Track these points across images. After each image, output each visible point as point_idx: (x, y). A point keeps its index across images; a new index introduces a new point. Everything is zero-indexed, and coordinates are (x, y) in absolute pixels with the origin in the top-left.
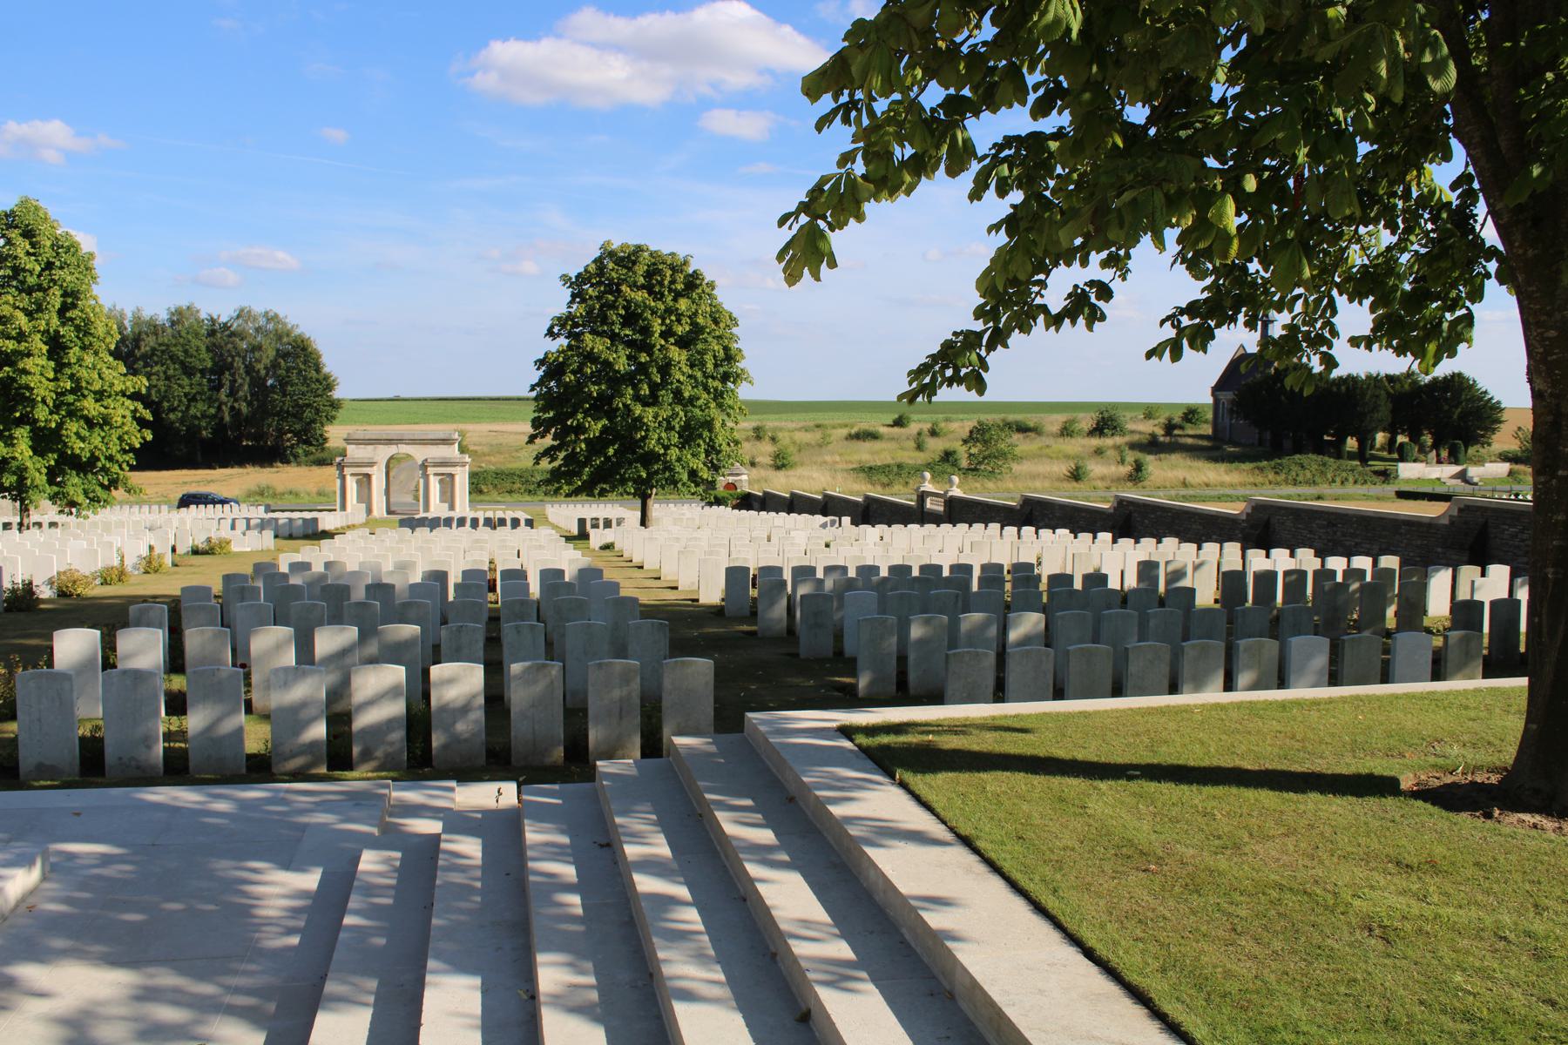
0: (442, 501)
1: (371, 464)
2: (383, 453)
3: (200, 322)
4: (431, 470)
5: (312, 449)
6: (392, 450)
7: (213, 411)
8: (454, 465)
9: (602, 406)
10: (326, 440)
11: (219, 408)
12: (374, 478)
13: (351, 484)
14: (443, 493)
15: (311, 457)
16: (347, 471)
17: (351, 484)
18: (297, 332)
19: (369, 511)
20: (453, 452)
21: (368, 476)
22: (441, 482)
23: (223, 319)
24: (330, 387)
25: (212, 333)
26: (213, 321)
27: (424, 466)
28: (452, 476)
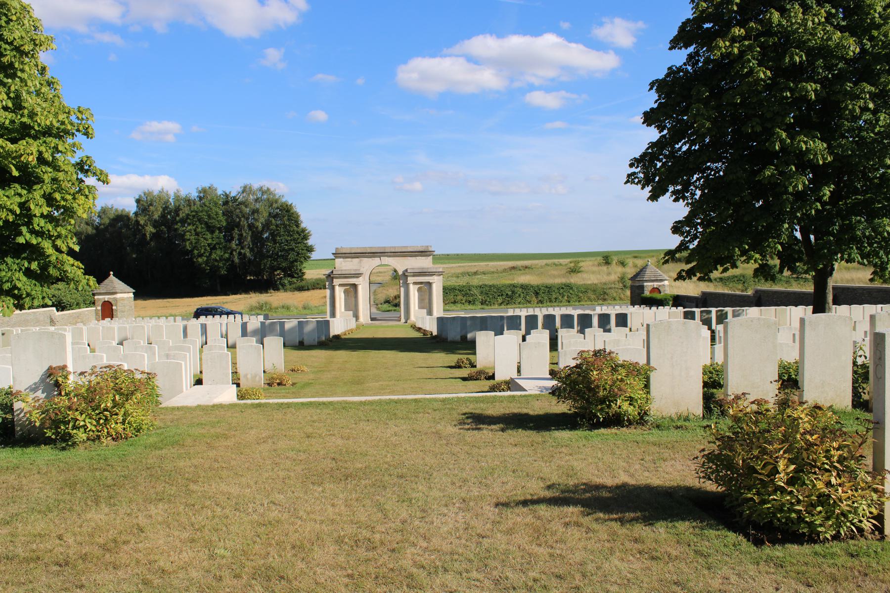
0: (421, 307)
1: (357, 275)
2: (367, 265)
3: (218, 197)
4: (411, 280)
5: (294, 280)
6: (376, 261)
7: (227, 255)
8: (431, 274)
9: (824, 118)
10: (303, 274)
11: (231, 253)
12: (360, 288)
13: (340, 293)
14: (421, 300)
15: (294, 286)
16: (336, 282)
17: (340, 293)
18: (284, 200)
19: (356, 316)
20: (425, 263)
21: (355, 286)
22: (419, 290)
23: (233, 194)
24: (306, 237)
25: (226, 203)
26: (227, 196)
27: (405, 275)
28: (429, 284)
